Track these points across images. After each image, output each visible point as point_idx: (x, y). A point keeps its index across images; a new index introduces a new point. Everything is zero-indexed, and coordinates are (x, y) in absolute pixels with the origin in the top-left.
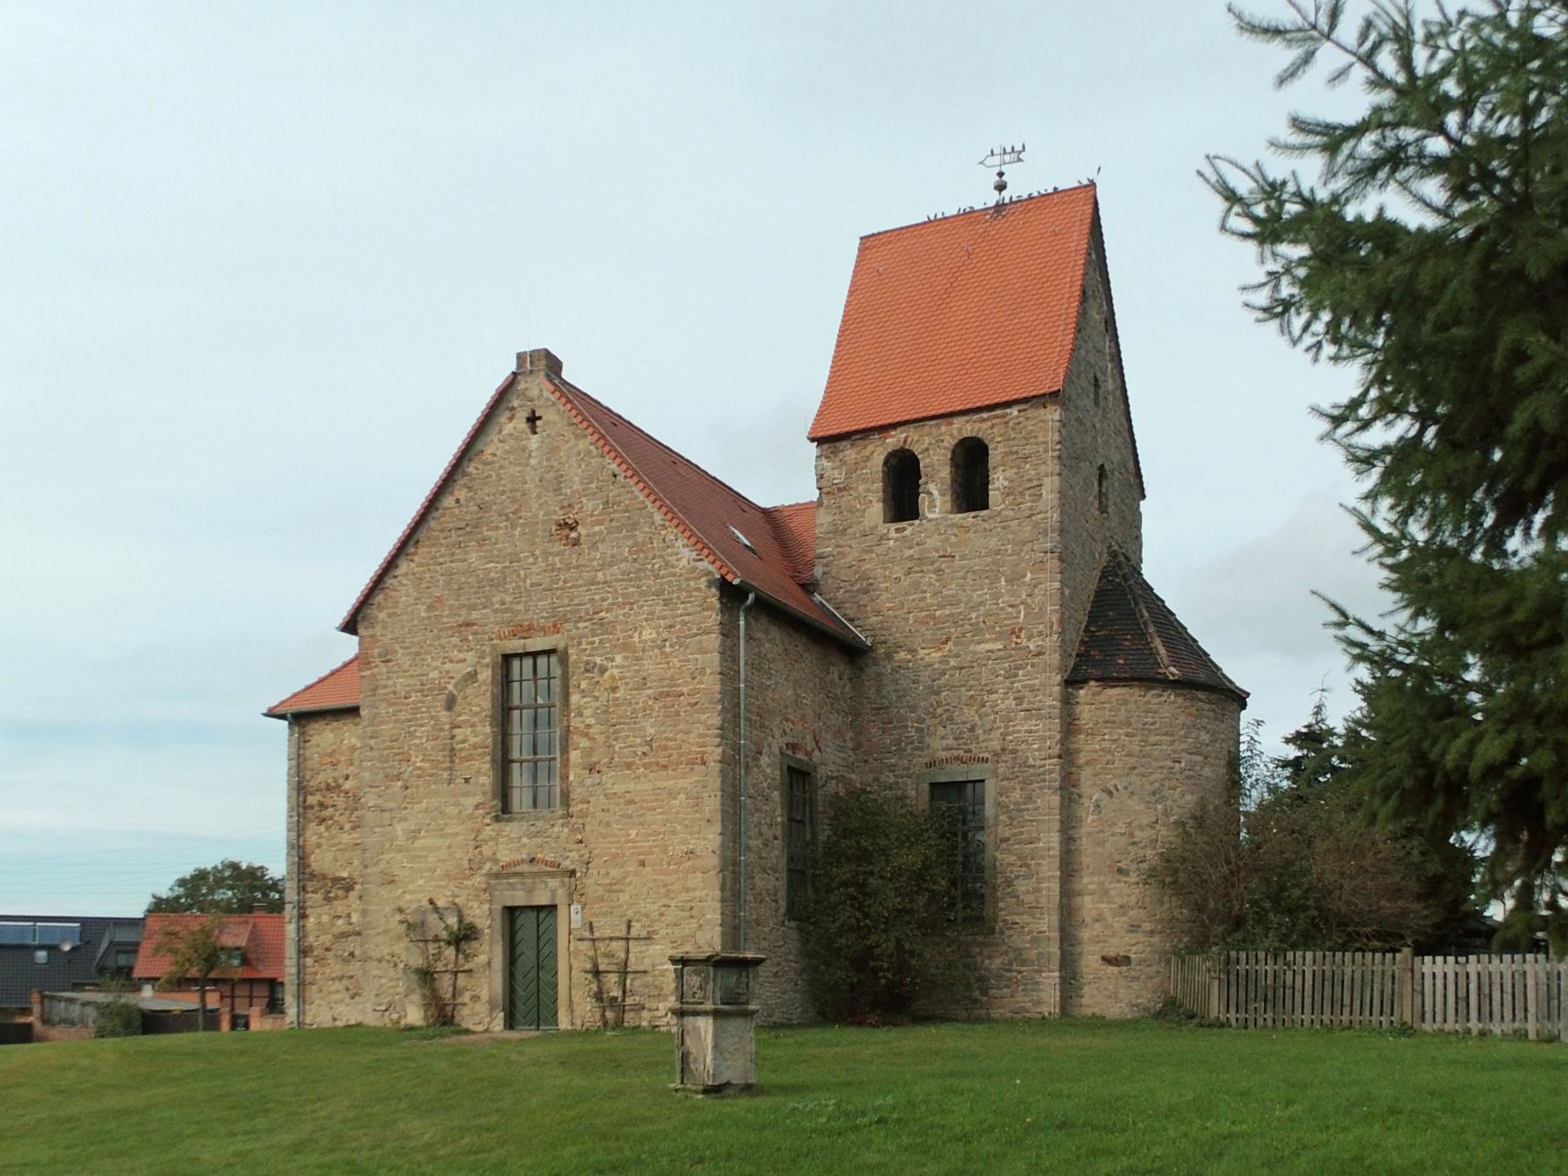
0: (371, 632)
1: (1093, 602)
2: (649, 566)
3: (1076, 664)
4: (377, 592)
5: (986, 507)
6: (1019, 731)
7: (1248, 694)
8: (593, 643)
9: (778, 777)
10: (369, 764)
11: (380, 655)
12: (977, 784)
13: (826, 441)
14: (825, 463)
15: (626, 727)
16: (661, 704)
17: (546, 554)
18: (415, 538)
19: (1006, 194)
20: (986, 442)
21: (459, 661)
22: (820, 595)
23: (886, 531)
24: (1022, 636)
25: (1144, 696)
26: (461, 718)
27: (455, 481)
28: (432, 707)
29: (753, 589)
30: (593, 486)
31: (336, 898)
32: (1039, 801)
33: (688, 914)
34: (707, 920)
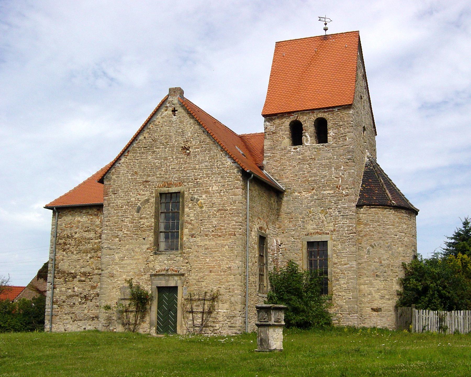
0: (109, 183)
1: (363, 175)
2: (216, 164)
3: (359, 199)
4: (112, 168)
5: (327, 142)
6: (340, 223)
7: (419, 210)
8: (194, 190)
9: (257, 240)
10: (106, 231)
11: (112, 192)
12: (324, 242)
13: (268, 117)
14: (268, 123)
15: (206, 221)
16: (219, 213)
17: (177, 158)
18: (128, 150)
19: (328, 33)
20: (326, 119)
21: (143, 195)
22: (266, 170)
23: (290, 149)
24: (340, 189)
25: (384, 211)
26: (143, 216)
27: (144, 131)
28: (131, 211)
30: (196, 135)
31: (69, 281)
32: (348, 249)
33: (228, 291)
34: (235, 293)
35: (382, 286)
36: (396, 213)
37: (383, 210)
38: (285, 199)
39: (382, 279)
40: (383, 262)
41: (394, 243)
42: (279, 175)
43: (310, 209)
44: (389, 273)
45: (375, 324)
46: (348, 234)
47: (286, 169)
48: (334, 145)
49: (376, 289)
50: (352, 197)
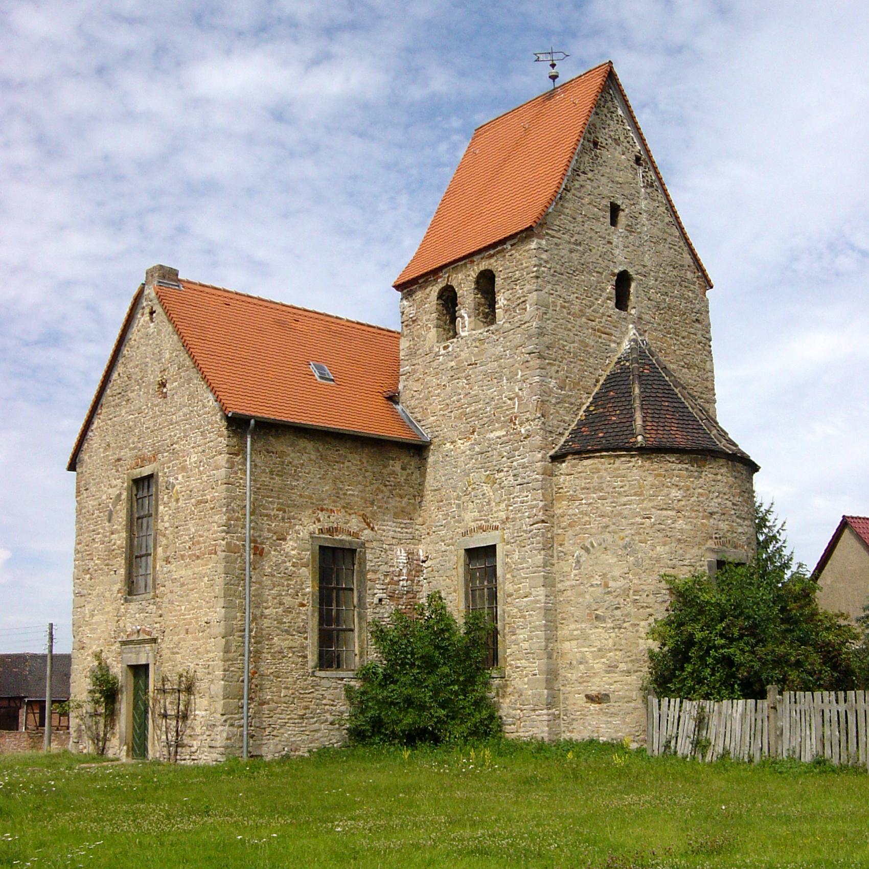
14: (405, 303)
19: (558, 82)
24: (517, 423)
25: (614, 463)
29: (253, 417)
35: (610, 640)
36: (647, 464)
37: (612, 461)
38: (431, 459)
39: (608, 626)
40: (611, 584)
41: (642, 538)
42: (421, 410)
43: (468, 476)
44: (628, 609)
45: (593, 731)
46: (531, 525)
47: (432, 394)
48: (507, 325)
49: (595, 649)
50: (536, 440)
